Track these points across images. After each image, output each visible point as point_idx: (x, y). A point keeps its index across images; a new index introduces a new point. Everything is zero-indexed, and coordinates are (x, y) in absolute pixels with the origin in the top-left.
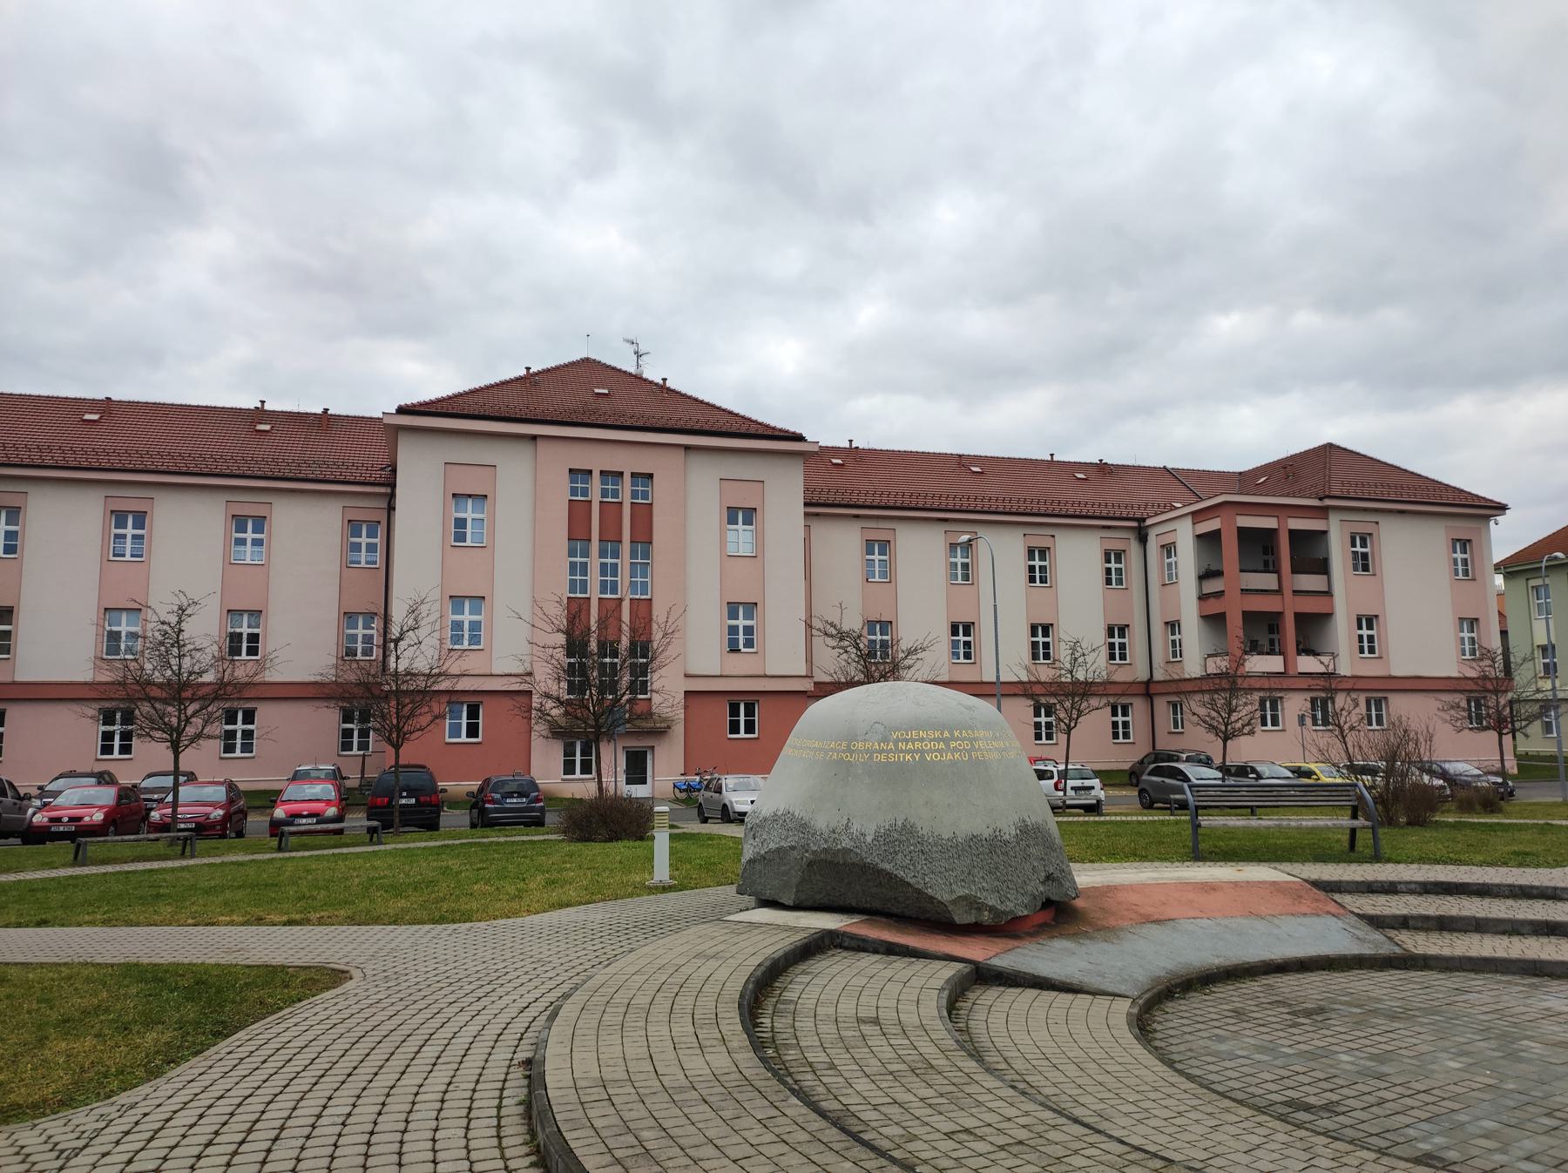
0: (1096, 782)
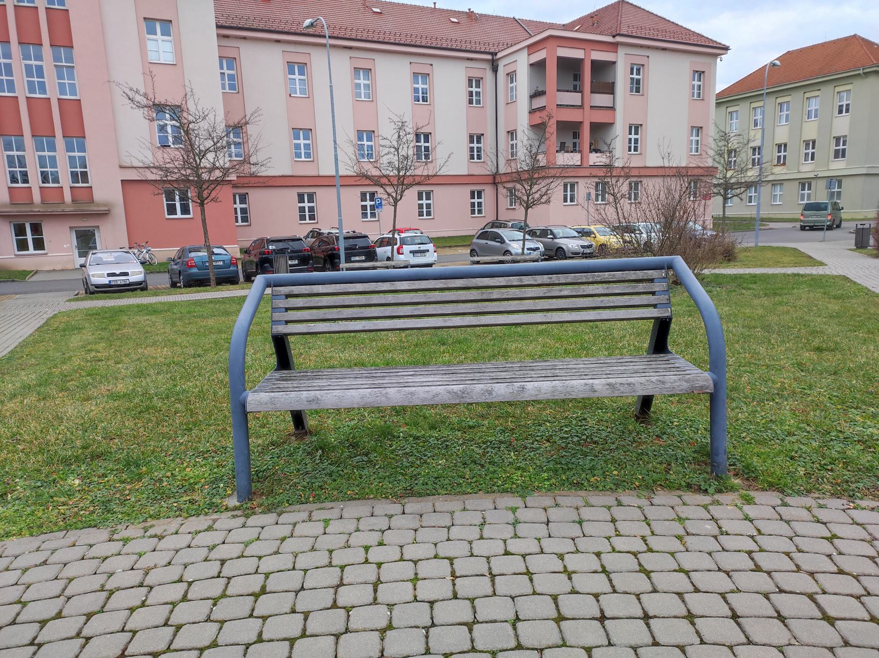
0: (430, 247)
